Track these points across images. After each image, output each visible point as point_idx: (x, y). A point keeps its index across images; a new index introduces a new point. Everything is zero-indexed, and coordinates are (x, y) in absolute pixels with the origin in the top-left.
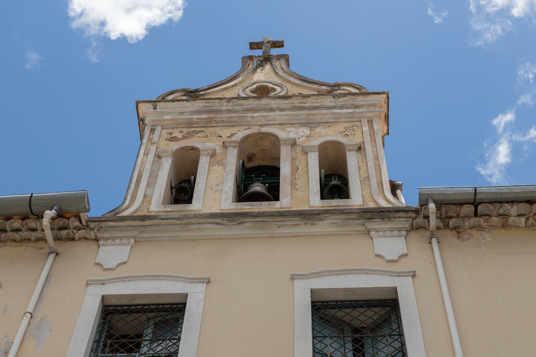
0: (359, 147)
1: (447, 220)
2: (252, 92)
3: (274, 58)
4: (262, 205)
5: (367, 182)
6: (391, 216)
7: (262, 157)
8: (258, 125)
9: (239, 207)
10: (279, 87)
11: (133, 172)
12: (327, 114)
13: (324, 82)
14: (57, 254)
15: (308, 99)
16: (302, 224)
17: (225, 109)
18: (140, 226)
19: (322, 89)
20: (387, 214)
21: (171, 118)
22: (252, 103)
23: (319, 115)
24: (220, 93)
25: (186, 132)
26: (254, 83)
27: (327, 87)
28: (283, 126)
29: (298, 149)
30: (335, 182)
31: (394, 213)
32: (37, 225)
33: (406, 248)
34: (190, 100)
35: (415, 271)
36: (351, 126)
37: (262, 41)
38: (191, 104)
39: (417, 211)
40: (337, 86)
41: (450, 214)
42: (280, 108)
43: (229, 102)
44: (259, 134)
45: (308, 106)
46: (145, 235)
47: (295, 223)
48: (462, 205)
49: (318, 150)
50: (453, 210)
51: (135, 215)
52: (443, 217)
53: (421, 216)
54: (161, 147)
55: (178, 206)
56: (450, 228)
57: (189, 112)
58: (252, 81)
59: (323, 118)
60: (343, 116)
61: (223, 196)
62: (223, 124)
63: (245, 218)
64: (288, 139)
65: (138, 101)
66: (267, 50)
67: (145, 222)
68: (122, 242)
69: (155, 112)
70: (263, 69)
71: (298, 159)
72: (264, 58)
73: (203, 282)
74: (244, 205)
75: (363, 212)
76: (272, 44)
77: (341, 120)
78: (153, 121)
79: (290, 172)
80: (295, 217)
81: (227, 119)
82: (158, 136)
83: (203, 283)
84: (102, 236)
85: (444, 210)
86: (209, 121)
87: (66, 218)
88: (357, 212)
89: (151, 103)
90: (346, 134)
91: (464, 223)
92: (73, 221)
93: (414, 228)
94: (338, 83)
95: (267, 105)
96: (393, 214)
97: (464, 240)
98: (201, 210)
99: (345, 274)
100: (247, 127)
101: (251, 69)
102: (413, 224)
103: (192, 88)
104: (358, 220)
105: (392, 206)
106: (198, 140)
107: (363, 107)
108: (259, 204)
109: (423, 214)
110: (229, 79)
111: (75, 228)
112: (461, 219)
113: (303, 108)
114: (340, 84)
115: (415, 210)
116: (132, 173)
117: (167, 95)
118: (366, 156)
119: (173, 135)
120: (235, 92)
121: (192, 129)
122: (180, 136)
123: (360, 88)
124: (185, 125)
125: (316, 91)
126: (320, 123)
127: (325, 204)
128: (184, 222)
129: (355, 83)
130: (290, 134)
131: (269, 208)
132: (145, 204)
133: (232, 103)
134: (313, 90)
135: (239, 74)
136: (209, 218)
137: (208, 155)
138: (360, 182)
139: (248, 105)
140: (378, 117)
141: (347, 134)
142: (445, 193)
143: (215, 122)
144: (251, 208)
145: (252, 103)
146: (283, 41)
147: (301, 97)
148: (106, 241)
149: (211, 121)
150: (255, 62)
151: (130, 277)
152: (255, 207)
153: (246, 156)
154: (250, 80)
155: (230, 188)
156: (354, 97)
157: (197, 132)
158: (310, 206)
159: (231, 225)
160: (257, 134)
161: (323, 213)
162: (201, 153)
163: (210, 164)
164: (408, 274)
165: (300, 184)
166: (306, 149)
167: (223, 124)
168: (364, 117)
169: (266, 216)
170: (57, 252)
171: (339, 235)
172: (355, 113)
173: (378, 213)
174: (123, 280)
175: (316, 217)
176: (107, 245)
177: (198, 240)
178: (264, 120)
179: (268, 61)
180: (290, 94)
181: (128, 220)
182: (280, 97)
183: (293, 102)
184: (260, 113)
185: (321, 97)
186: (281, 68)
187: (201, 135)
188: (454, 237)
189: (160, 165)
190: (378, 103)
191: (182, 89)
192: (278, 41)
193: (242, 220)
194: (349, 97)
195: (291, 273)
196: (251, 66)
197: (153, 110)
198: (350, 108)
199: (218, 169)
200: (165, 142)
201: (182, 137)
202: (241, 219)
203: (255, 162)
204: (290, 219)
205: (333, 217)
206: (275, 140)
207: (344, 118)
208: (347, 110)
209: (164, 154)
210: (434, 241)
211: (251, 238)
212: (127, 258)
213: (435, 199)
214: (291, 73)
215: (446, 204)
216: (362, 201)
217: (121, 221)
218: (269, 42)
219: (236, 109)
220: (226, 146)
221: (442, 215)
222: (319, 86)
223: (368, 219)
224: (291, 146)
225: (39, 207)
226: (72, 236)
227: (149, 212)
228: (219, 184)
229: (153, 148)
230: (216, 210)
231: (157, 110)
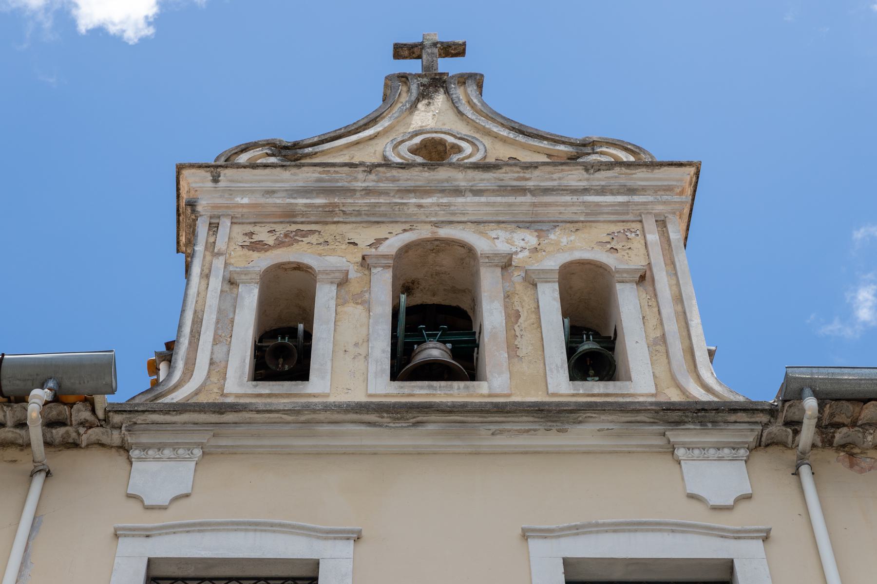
0: (641, 276)
1: (832, 431)
2: (414, 151)
3: (452, 80)
4: (451, 387)
5: (661, 348)
6: (720, 419)
7: (430, 287)
8: (431, 222)
9: (406, 390)
10: (468, 144)
11: (181, 312)
12: (573, 205)
13: (562, 137)
14: (48, 474)
15: (533, 171)
16: (539, 429)
17: (361, 187)
18: (213, 423)
19: (558, 150)
20: (713, 414)
21: (251, 203)
22: (417, 176)
23: (557, 206)
24: (345, 152)
25: (282, 232)
26: (416, 134)
27: (569, 146)
28: (481, 227)
29: (517, 276)
30: (588, 345)
31: (727, 414)
32: (5, 416)
33: (749, 484)
34: (289, 166)
35: (770, 530)
36: (622, 231)
37: (421, 41)
38: (291, 174)
39: (772, 412)
40: (587, 146)
41: (837, 419)
42: (474, 188)
43: (370, 172)
44: (433, 242)
45: (534, 186)
46: (223, 442)
47: (527, 428)
48: (866, 401)
49: (557, 280)
50: (848, 409)
51: (191, 401)
52: (823, 424)
53: (781, 420)
54: (232, 261)
55: (282, 385)
56: (834, 447)
57: (287, 190)
58: (408, 128)
59: (564, 213)
60: (606, 210)
61: (372, 368)
62: (359, 219)
63: (427, 413)
64: (496, 255)
65: (181, 164)
66: (432, 62)
67: (223, 416)
68: (177, 453)
69: (216, 187)
70: (430, 103)
71: (517, 297)
72: (431, 79)
73: (348, 539)
74: (414, 387)
75: (664, 410)
76: (442, 49)
77: (601, 218)
78: (212, 207)
79: (504, 322)
80: (526, 416)
81: (366, 208)
82: (227, 240)
83: (348, 541)
84: (138, 441)
85: (828, 411)
86: (329, 211)
87: (65, 404)
88: (653, 410)
89: (208, 169)
90: (612, 248)
91: (864, 437)
92: (79, 411)
93: (763, 444)
94: (590, 138)
95: (447, 181)
96: (724, 416)
97: (862, 471)
98: (327, 396)
99: (630, 531)
100: (407, 226)
101: (406, 102)
102: (762, 435)
103: (288, 138)
104: (652, 426)
105: (719, 400)
106: (309, 251)
107: (646, 191)
108: (446, 387)
109: (785, 417)
110: (361, 123)
111: (82, 424)
112: (860, 429)
113: (523, 191)
114: (594, 141)
115: (770, 410)
116: (181, 315)
117: (236, 153)
118: (656, 295)
119: (256, 238)
120: (376, 151)
121: (294, 227)
122: (270, 240)
123: (637, 150)
124: (280, 218)
125: (545, 154)
126: (557, 222)
127: (580, 390)
128: (303, 418)
129: (626, 140)
130: (497, 244)
131: (466, 394)
132: (214, 379)
133: (376, 175)
134: (539, 153)
135: (383, 113)
136: (354, 413)
137: (332, 283)
138: (647, 346)
139: (408, 180)
140: (678, 213)
141: (615, 248)
142: (838, 379)
143: (342, 214)
144: (430, 394)
145: (417, 176)
146: (464, 44)
147: (520, 166)
148: (144, 451)
149: (334, 211)
150: (414, 87)
151: (201, 524)
152: (439, 392)
153: (401, 285)
154: (404, 126)
155: (383, 351)
156: (628, 171)
157: (304, 232)
158: (549, 392)
159: (397, 427)
160: (428, 241)
161: (583, 410)
162: (319, 277)
163: (338, 300)
164: (756, 535)
165: (525, 345)
166: (533, 276)
167: (359, 219)
168: (648, 213)
169: (469, 412)
170: (49, 471)
171: (611, 453)
172: (631, 205)
173: (694, 412)
174: (188, 529)
175: (568, 417)
176: (161, 458)
177: (328, 454)
178: (442, 212)
179: (439, 87)
180: (491, 160)
181: (190, 411)
182: (475, 166)
183: (501, 176)
184: (436, 198)
185: (560, 168)
186: (469, 102)
187: (313, 239)
188: (843, 464)
189: (235, 299)
190: (676, 185)
191: (265, 141)
192: (454, 42)
193: (419, 419)
194: (619, 170)
195: (523, 526)
196: (404, 98)
197: (211, 184)
198: (619, 193)
199: (354, 311)
200: (240, 252)
201: (274, 244)
202: (418, 417)
203: (415, 297)
204: (516, 419)
205: (603, 417)
206: (466, 255)
207: (608, 213)
208: (614, 197)
209: (243, 277)
210: (805, 470)
211: (435, 453)
212: (190, 489)
213: (818, 389)
214: (492, 114)
215: (832, 400)
216: (654, 386)
217: (175, 413)
218: (435, 44)
219: (383, 188)
220: (368, 265)
221: (822, 420)
222: (551, 145)
223: (672, 424)
224: (502, 268)
225: (18, 382)
226: (73, 439)
227: (223, 395)
228: (360, 342)
229: (219, 264)
230: (360, 397)
231: (221, 184)
